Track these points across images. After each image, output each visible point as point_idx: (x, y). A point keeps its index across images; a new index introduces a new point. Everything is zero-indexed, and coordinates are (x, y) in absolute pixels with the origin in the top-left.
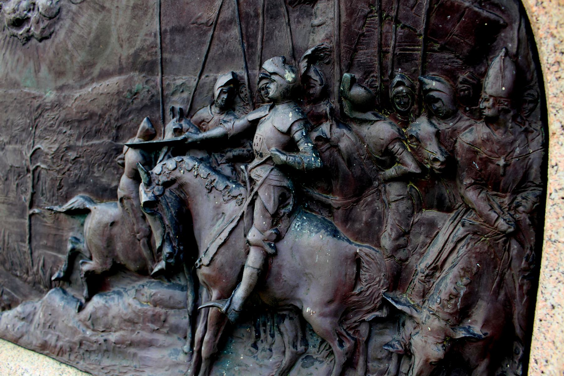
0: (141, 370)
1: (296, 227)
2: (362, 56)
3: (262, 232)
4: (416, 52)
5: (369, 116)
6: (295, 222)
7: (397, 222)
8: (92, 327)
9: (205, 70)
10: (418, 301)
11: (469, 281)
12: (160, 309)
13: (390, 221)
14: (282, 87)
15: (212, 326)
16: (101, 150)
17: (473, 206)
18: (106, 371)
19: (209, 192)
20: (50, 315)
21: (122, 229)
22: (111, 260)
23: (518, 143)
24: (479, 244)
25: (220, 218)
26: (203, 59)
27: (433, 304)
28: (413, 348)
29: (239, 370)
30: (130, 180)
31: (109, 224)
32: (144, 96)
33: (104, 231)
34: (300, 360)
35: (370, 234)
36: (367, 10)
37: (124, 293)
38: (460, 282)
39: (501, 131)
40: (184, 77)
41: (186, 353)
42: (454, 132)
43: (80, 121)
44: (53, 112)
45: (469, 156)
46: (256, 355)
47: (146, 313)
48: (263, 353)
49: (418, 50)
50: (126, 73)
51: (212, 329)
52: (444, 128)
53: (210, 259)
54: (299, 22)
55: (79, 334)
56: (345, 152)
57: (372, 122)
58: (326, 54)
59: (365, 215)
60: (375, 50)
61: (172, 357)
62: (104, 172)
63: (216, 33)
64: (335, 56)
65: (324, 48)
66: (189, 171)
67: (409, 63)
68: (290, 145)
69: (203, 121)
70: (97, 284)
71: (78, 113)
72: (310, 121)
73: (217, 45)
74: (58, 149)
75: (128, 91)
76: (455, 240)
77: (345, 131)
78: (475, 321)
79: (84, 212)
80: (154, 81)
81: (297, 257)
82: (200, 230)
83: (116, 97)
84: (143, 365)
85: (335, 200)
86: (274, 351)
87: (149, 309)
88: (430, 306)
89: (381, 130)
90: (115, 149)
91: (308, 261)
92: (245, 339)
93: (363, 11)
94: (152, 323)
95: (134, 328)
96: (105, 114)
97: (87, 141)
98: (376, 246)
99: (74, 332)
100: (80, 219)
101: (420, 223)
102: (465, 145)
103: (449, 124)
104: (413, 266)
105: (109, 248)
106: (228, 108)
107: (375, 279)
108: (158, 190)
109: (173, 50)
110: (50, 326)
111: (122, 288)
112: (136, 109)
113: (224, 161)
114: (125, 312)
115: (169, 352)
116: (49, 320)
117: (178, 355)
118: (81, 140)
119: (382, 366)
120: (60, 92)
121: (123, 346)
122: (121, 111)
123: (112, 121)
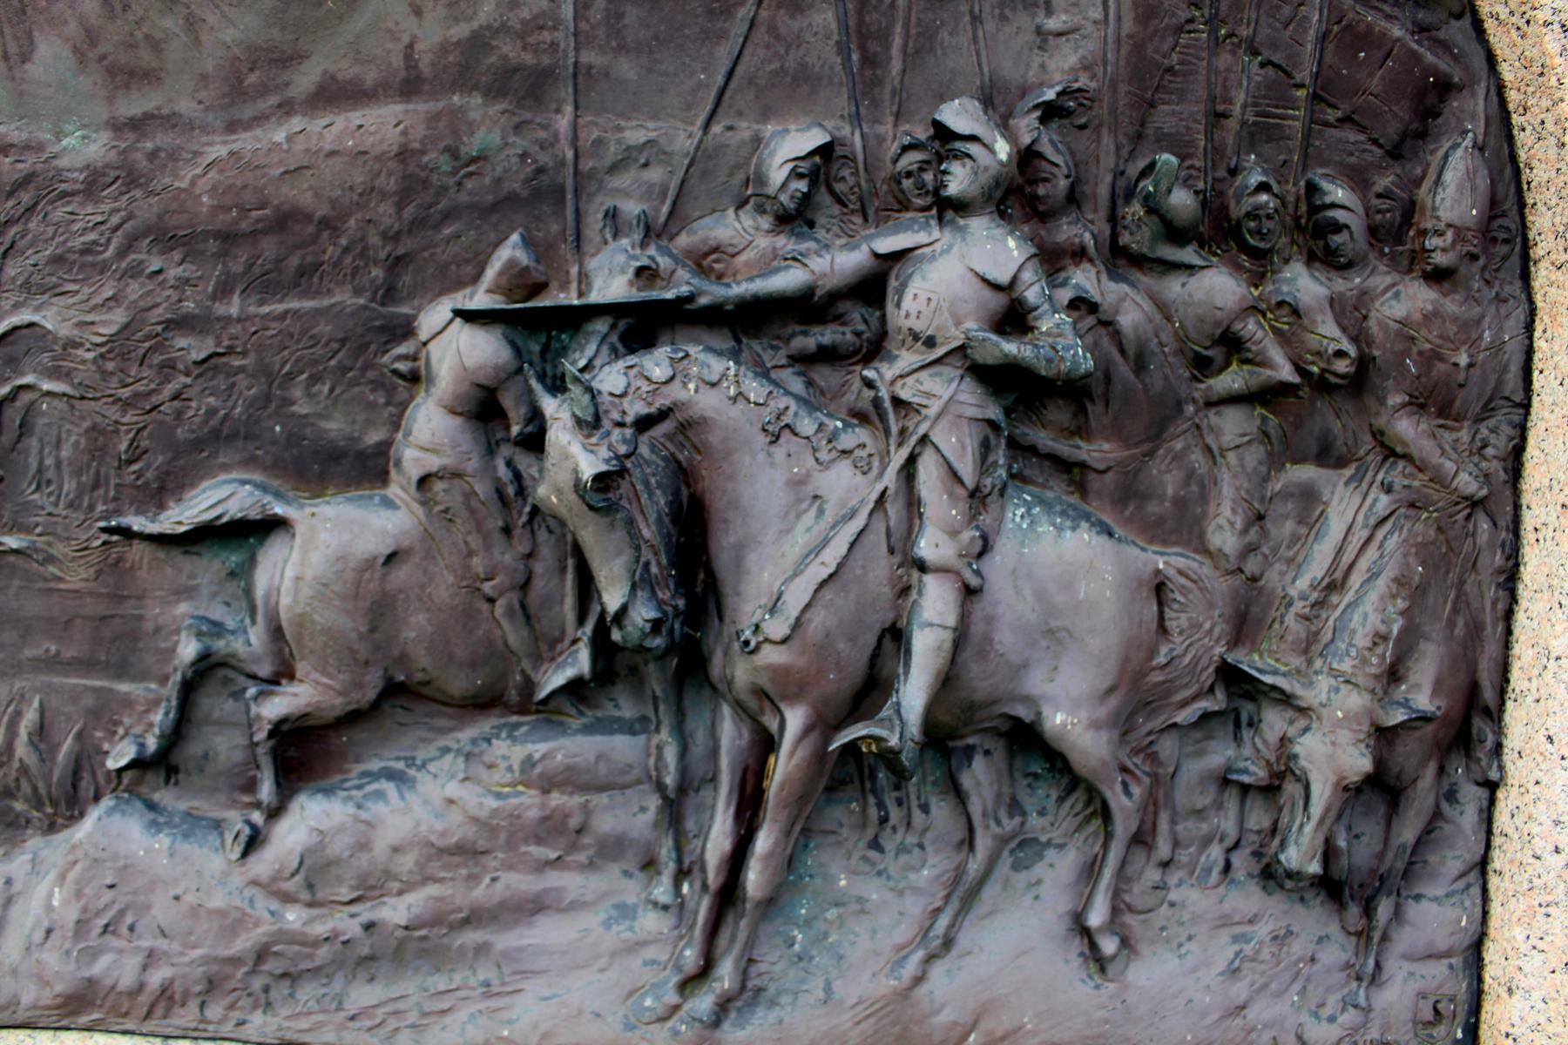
0: (510, 989)
1: (1018, 519)
2: (1165, 118)
3: (954, 533)
4: (1290, 122)
5: (1188, 255)
6: (1010, 508)
7: (1243, 493)
8: (305, 896)
9: (720, 110)
10: (1297, 661)
11: (1407, 603)
12: (565, 798)
13: (1227, 491)
14: (987, 174)
15: (785, 807)
16: (324, 329)
17: (1407, 450)
18: (368, 1023)
19: (772, 443)
20: (111, 887)
21: (425, 571)
22: (381, 672)
23: (1487, 319)
24: (1419, 527)
25: (806, 511)
26: (720, 79)
27: (1341, 660)
28: (1303, 762)
29: (840, 916)
30: (458, 421)
31: (381, 560)
32: (505, 170)
33: (358, 584)
34: (1006, 853)
35: (1182, 525)
36: (1184, 15)
37: (412, 772)
38: (1391, 609)
39: (1458, 297)
40: (651, 125)
41: (666, 908)
42: (1365, 296)
43: (229, 238)
44: (97, 202)
45: (1399, 346)
46: (882, 866)
47: (519, 817)
48: (904, 858)
49: (1294, 118)
50: (434, 96)
51: (783, 817)
52: (1342, 289)
53: (792, 621)
54: (1003, 18)
55: (256, 925)
56: (1132, 336)
57: (1190, 268)
58: (1081, 105)
59: (1171, 484)
60: (1198, 109)
61: (615, 928)
62: (336, 401)
63: (764, 14)
64: (1102, 110)
65: (1079, 90)
66: (713, 385)
67: (1273, 145)
68: (1014, 318)
69: (716, 249)
70: (302, 754)
71: (217, 209)
72: (1052, 260)
73: (768, 46)
74: (126, 326)
75: (447, 149)
76: (1372, 521)
77: (1125, 288)
78: (1417, 687)
79: (256, 530)
80: (546, 127)
81: (1027, 593)
82: (740, 548)
83: (392, 165)
84: (516, 973)
85: (1097, 451)
86: (929, 848)
87: (529, 803)
88: (1335, 666)
89: (1216, 287)
90: (382, 328)
91: (1060, 599)
92: (845, 832)
93: (1174, 15)
94: (540, 841)
95: (476, 870)
96: (343, 217)
97: (262, 303)
98: (1196, 551)
99: (234, 923)
100: (224, 555)
101: (1286, 495)
102: (1392, 324)
103: (1352, 280)
104: (1274, 589)
105: (378, 636)
106: (794, 219)
107: (1201, 626)
108: (624, 441)
109: (614, 44)
110: (107, 926)
111: (398, 759)
112: (473, 206)
113: (784, 361)
114: (439, 826)
115: (603, 916)
116: (107, 907)
117: (634, 918)
118: (236, 299)
119: (1204, 826)
120: (131, 136)
121: (435, 930)
122: (410, 211)
123: (374, 240)
